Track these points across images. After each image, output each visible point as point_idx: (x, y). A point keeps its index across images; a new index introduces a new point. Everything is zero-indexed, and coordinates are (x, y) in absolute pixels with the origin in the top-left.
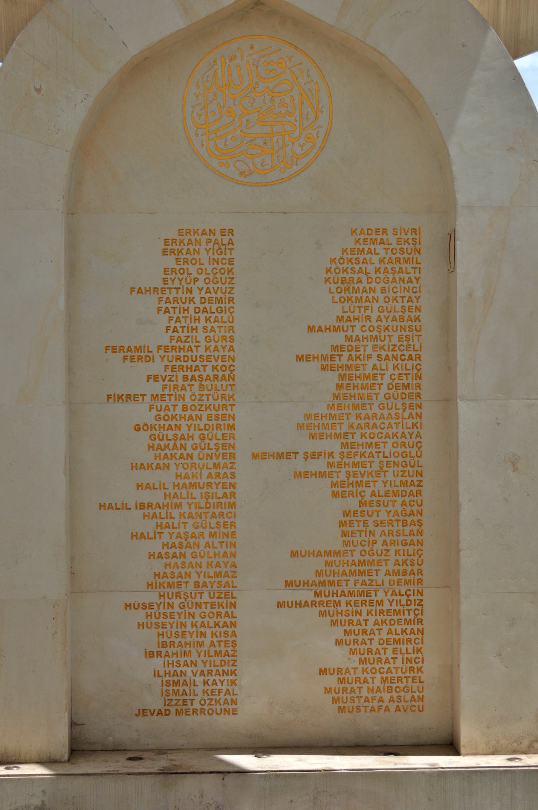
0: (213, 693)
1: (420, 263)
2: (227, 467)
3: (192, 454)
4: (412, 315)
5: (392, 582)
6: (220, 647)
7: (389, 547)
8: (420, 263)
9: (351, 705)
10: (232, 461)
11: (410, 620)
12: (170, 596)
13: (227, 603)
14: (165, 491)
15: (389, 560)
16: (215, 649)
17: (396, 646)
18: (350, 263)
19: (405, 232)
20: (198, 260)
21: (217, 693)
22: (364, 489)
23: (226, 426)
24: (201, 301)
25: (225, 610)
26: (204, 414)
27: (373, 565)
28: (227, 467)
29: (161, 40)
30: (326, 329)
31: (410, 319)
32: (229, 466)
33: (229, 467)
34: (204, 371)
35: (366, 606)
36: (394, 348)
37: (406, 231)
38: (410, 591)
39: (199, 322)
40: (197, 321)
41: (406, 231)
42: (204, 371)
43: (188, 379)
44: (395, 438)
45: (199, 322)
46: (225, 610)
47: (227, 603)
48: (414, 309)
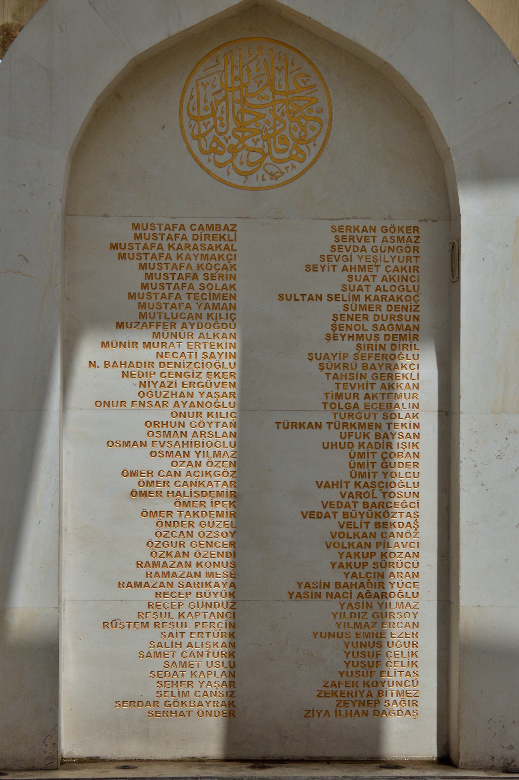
0: (348, 685)
1: (236, 250)
4: (395, 294)
5: (377, 318)
7: (380, 303)
8: (236, 250)
9: (158, 272)
11: (365, 472)
15: (375, 384)
18: (357, 557)
21: (367, 358)
22: (367, 312)
27: (151, 278)
29: (386, 63)
31: (366, 278)
32: (413, 239)
34: (374, 281)
35: (210, 240)
42: (374, 281)
43: (368, 368)
44: (392, 281)
48: (138, 404)
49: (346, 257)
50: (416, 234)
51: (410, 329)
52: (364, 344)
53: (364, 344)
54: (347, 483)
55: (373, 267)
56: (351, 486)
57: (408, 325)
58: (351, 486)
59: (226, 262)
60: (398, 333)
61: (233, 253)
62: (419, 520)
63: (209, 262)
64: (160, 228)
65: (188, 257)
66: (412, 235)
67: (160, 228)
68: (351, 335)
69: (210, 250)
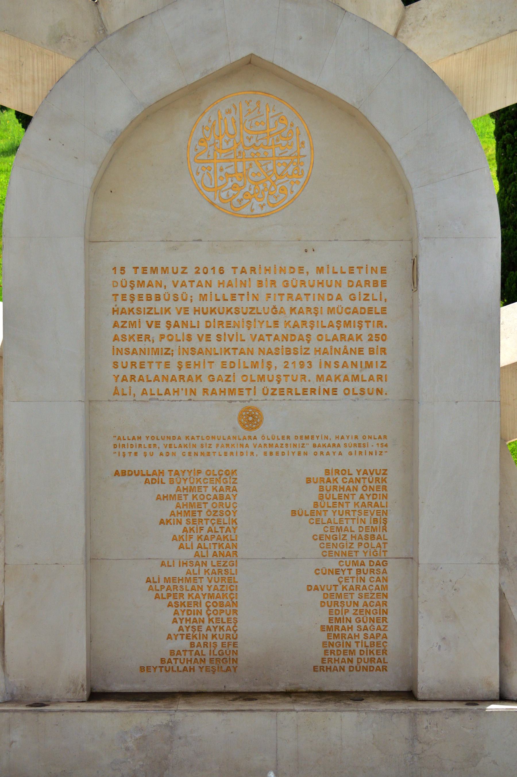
2: (380, 629)
3: (358, 602)
6: (215, 549)
8: (237, 582)
10: (385, 624)
12: (365, 572)
13: (200, 634)
14: (352, 533)
16: (202, 592)
17: (329, 632)
19: (230, 338)
20: (347, 470)
23: (381, 495)
24: (348, 284)
25: (198, 641)
26: (360, 486)
28: (380, 629)
30: (164, 497)
32: (382, 628)
33: (382, 629)
36: (252, 311)
37: (231, 336)
38: (319, 570)
39: (352, 630)
40: (350, 630)
41: (231, 336)
45: (352, 630)
46: (198, 641)
47: (200, 634)
49: (353, 296)
50: (385, 624)
51: (379, 605)
52: (343, 642)
53: (343, 642)
54: (336, 586)
55: (353, 552)
56: (340, 588)
57: (378, 577)
58: (340, 588)
59: (229, 600)
60: (375, 492)
61: (235, 585)
62: (387, 526)
63: (215, 600)
64: (235, 352)
65: (198, 596)
66: (381, 625)
67: (235, 352)
68: (329, 667)
69: (216, 591)
